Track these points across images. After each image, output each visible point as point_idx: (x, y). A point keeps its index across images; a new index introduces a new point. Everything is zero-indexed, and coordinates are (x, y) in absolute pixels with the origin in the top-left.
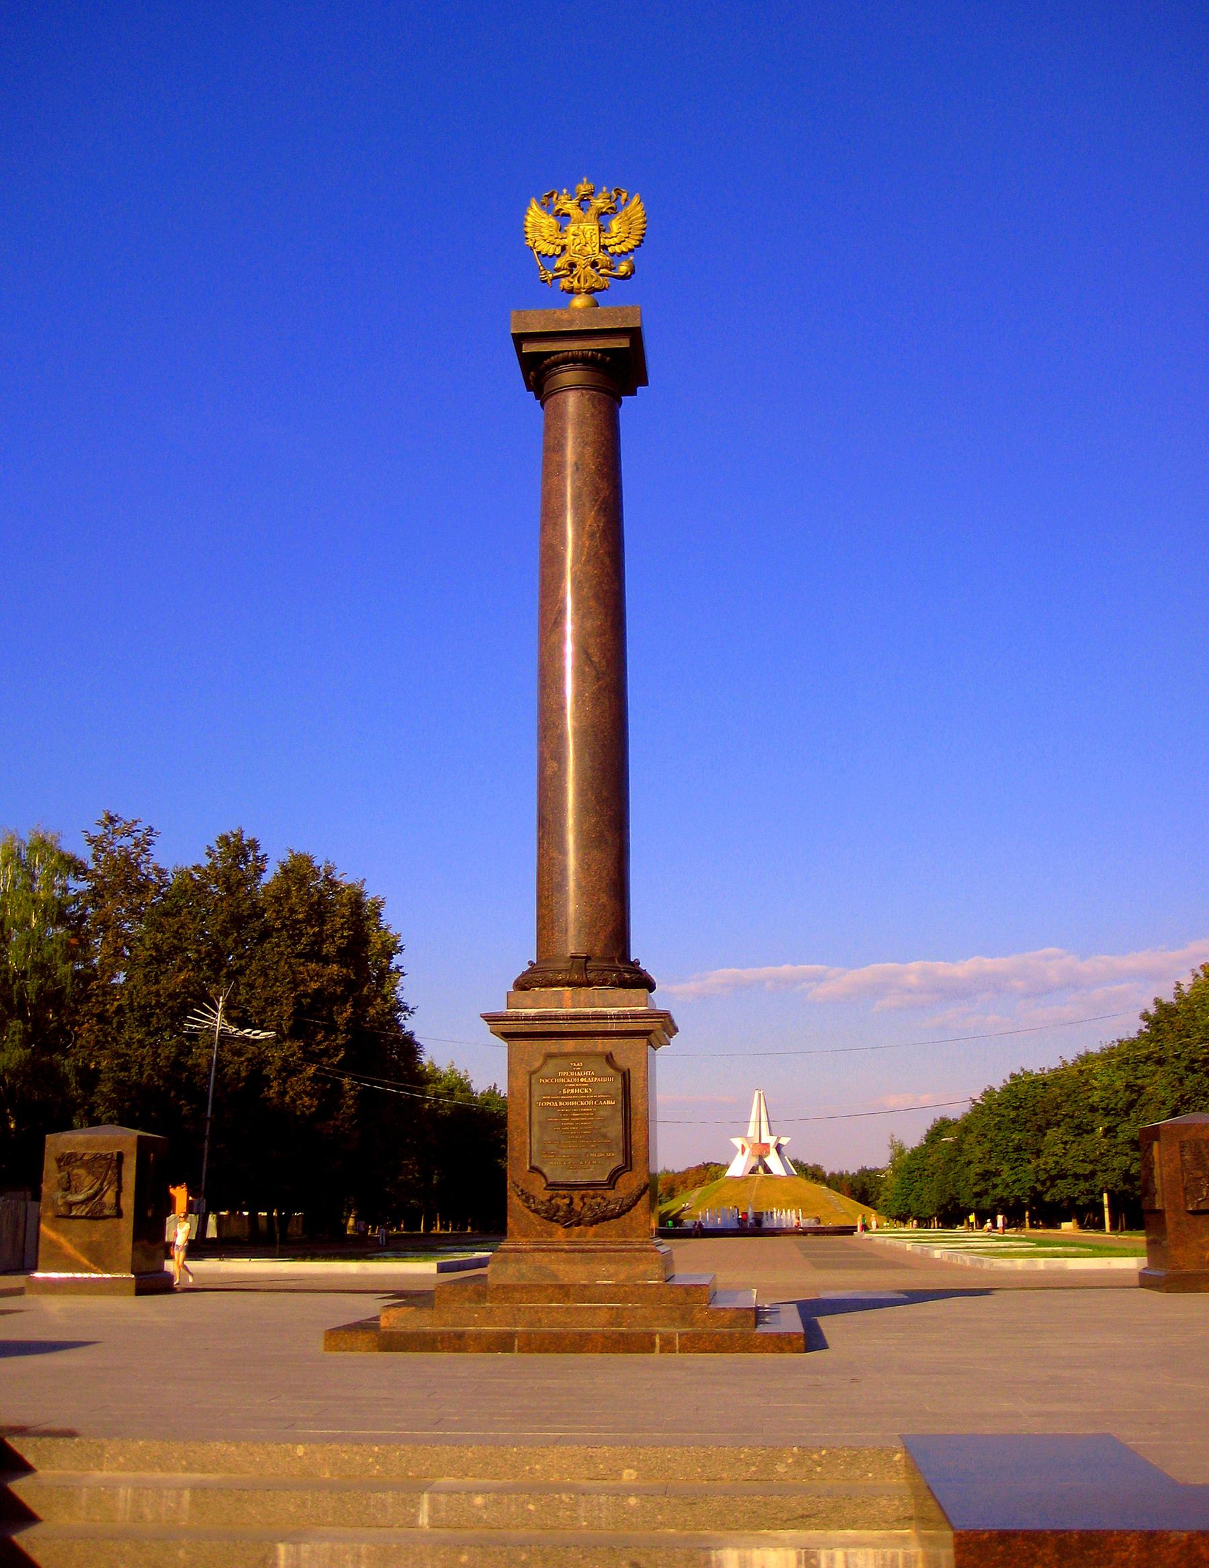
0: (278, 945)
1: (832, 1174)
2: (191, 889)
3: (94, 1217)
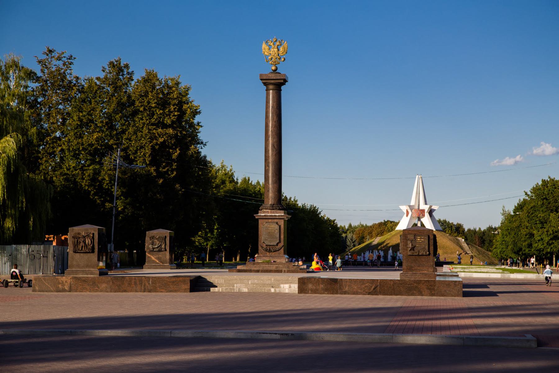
0: (142, 119)
1: (469, 230)
2: (90, 93)
3: (160, 251)
